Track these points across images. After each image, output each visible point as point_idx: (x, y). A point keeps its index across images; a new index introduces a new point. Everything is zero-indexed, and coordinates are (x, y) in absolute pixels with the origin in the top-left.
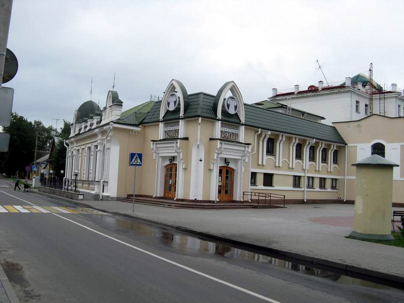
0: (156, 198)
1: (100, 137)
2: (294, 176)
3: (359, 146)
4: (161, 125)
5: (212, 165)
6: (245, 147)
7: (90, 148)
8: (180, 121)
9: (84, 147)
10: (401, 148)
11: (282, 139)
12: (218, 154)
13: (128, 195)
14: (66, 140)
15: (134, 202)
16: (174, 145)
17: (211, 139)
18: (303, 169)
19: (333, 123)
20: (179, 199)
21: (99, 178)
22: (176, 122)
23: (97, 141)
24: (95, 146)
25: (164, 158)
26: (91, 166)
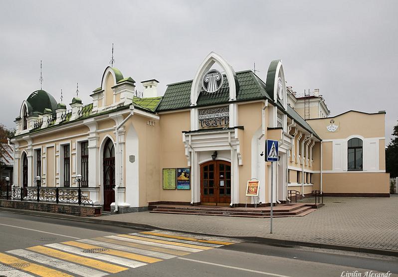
3: (335, 141)
4: (194, 113)
7: (66, 147)
8: (231, 106)
14: (11, 138)
15: (272, 216)
22: (187, 111)
23: (88, 135)
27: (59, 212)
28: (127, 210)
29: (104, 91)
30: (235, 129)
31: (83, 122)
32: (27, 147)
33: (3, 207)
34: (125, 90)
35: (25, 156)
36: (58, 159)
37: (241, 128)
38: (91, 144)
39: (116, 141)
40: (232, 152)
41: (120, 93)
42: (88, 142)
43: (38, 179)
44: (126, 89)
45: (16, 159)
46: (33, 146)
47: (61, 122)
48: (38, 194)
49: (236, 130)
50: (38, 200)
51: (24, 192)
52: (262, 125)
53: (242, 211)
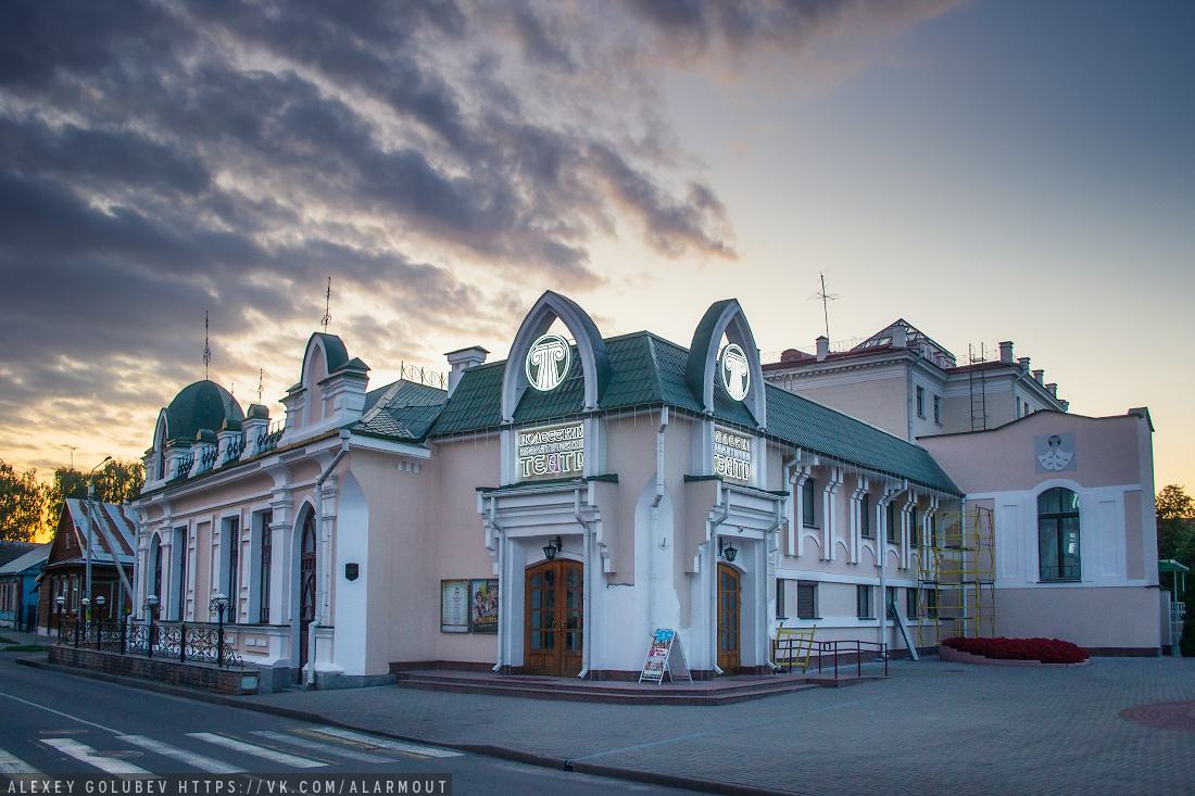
0: (505, 669)
1: (280, 482)
2: (858, 586)
5: (696, 559)
6: (775, 501)
7: (233, 523)
9: (208, 517)
10: (1125, 496)
11: (837, 478)
12: (714, 525)
13: (392, 665)
16: (575, 498)
17: (688, 479)
18: (876, 566)
19: (917, 438)
20: (596, 672)
21: (284, 616)
23: (271, 496)
24: (256, 513)
25: (522, 541)
26: (511, 574)
27: (182, 683)
28: (338, 681)
29: (306, 389)
30: (590, 483)
31: (259, 465)
32: (161, 522)
33: (84, 666)
34: (341, 389)
35: (157, 539)
36: (218, 551)
37: (611, 479)
38: (279, 518)
39: (325, 508)
40: (586, 539)
41: (334, 396)
42: (271, 513)
43: (152, 602)
44: (346, 388)
45: (141, 550)
46: (174, 519)
47: (227, 463)
48: (183, 640)
49: (591, 485)
50: (183, 656)
51: (153, 636)
52: (656, 473)
53: (621, 689)
